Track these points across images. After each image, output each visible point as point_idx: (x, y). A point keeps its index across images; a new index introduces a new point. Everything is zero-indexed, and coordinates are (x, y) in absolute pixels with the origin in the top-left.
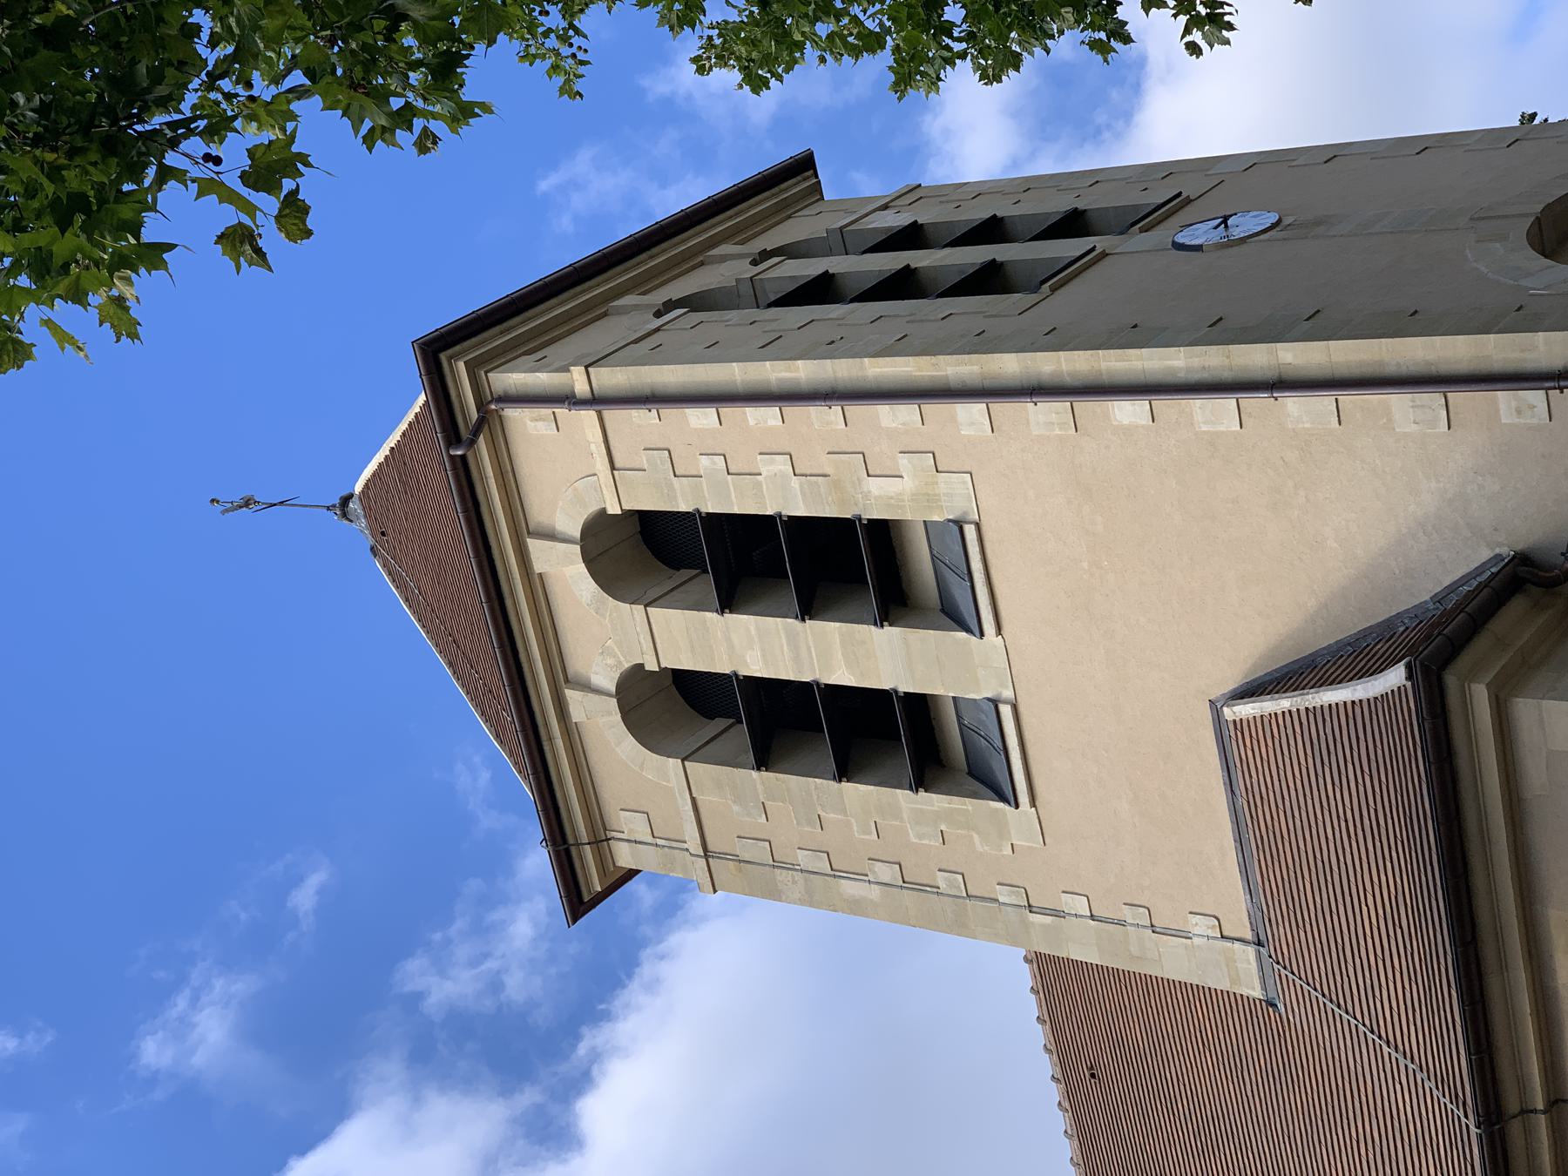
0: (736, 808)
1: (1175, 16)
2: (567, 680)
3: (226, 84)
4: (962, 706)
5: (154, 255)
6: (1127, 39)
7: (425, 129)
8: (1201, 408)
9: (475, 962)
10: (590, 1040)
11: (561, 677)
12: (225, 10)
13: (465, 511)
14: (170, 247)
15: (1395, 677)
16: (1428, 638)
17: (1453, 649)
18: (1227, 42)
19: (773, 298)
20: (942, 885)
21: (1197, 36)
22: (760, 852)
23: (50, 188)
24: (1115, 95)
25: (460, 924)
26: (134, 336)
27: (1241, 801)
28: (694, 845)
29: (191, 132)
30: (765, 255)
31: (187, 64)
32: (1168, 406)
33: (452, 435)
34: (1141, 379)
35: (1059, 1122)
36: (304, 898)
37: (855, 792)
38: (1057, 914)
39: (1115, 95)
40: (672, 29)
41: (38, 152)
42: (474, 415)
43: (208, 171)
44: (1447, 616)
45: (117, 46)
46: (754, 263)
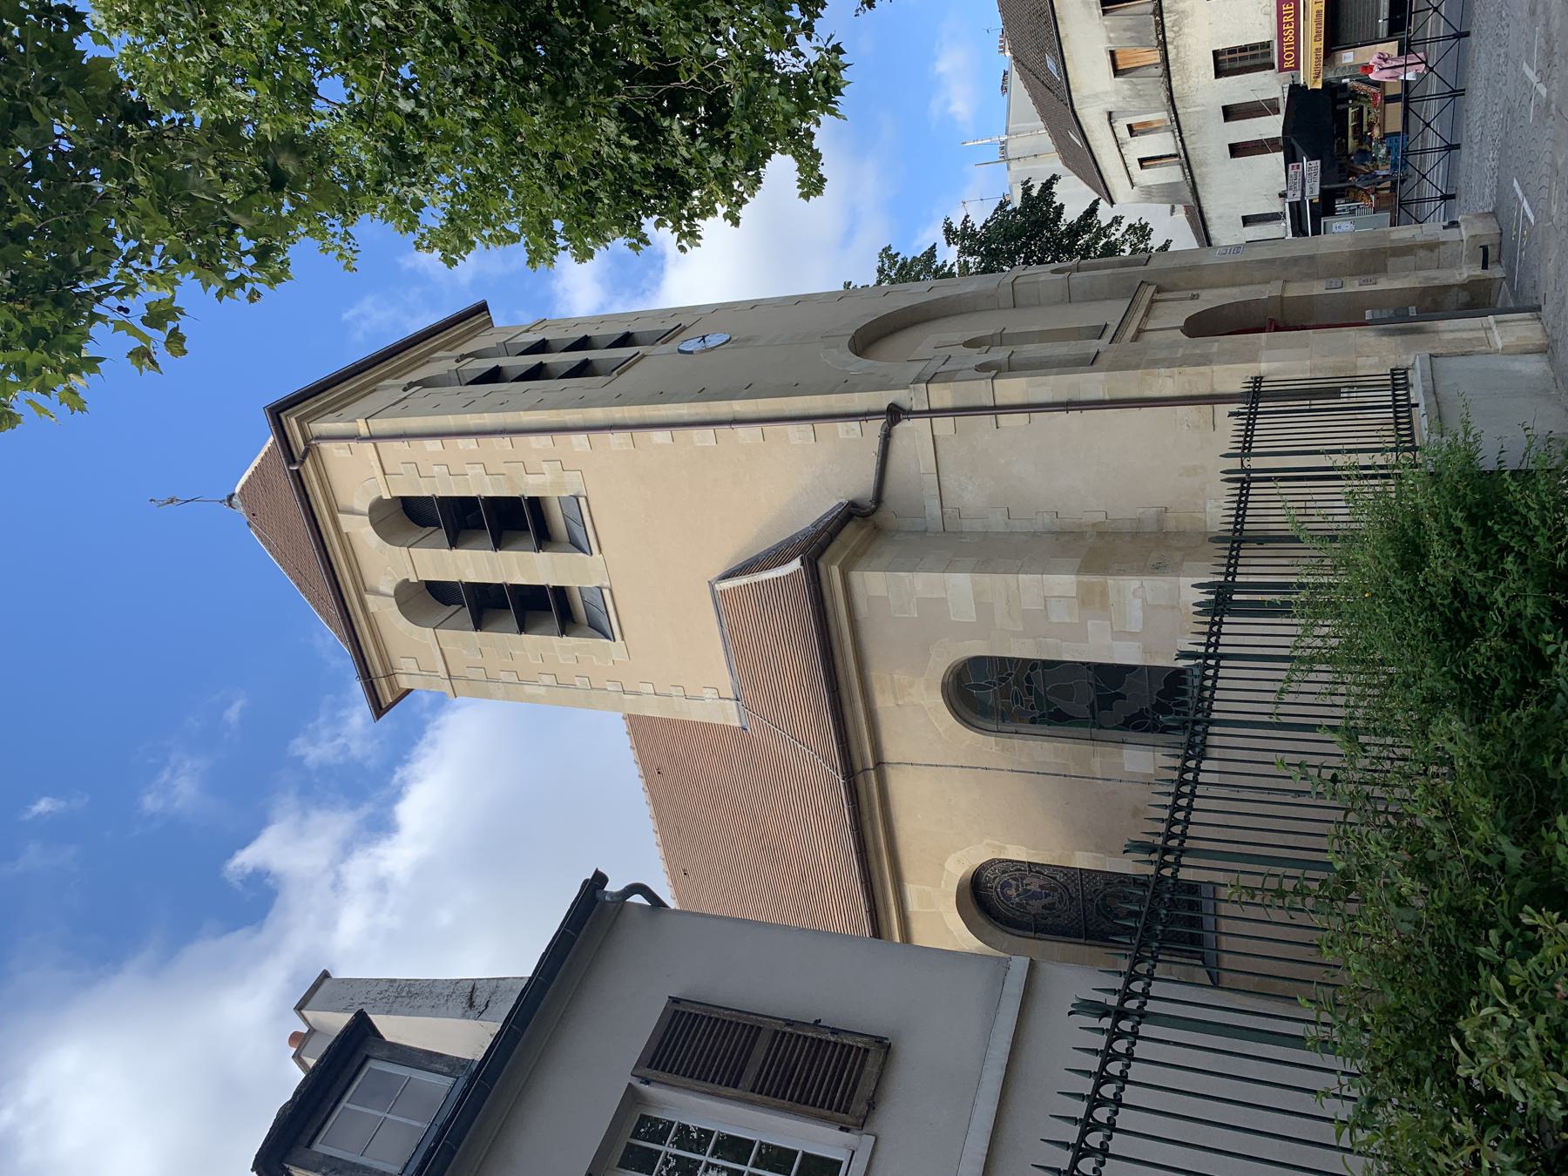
0: (465, 652)
1: (672, 232)
2: (366, 590)
3: (135, 264)
4: (583, 591)
5: (92, 363)
6: (648, 243)
7: (253, 289)
8: (696, 433)
9: (332, 739)
10: (400, 773)
11: (362, 589)
12: (123, 221)
13: (301, 500)
14: (101, 359)
15: (795, 565)
16: (810, 545)
17: (822, 549)
18: (699, 245)
19: (469, 380)
20: (577, 683)
21: (684, 243)
22: (480, 674)
23: (20, 327)
24: (651, 273)
25: (322, 719)
26: (82, 410)
27: (726, 631)
28: (443, 673)
29: (109, 293)
30: (463, 357)
31: (109, 252)
32: (680, 433)
33: (291, 460)
34: (665, 420)
35: (644, 797)
36: (233, 714)
37: (530, 640)
38: (637, 693)
39: (651, 273)
40: (401, 232)
41: (11, 304)
42: (303, 448)
43: (121, 316)
44: (819, 533)
45: (63, 240)
46: (457, 361)
